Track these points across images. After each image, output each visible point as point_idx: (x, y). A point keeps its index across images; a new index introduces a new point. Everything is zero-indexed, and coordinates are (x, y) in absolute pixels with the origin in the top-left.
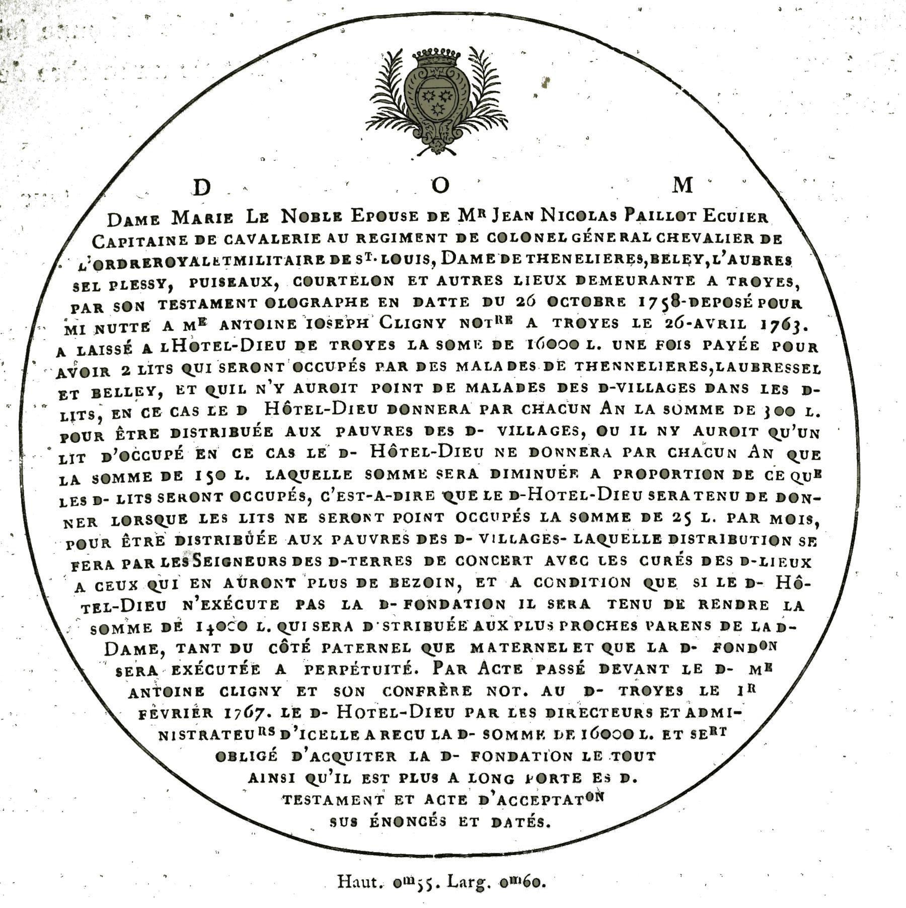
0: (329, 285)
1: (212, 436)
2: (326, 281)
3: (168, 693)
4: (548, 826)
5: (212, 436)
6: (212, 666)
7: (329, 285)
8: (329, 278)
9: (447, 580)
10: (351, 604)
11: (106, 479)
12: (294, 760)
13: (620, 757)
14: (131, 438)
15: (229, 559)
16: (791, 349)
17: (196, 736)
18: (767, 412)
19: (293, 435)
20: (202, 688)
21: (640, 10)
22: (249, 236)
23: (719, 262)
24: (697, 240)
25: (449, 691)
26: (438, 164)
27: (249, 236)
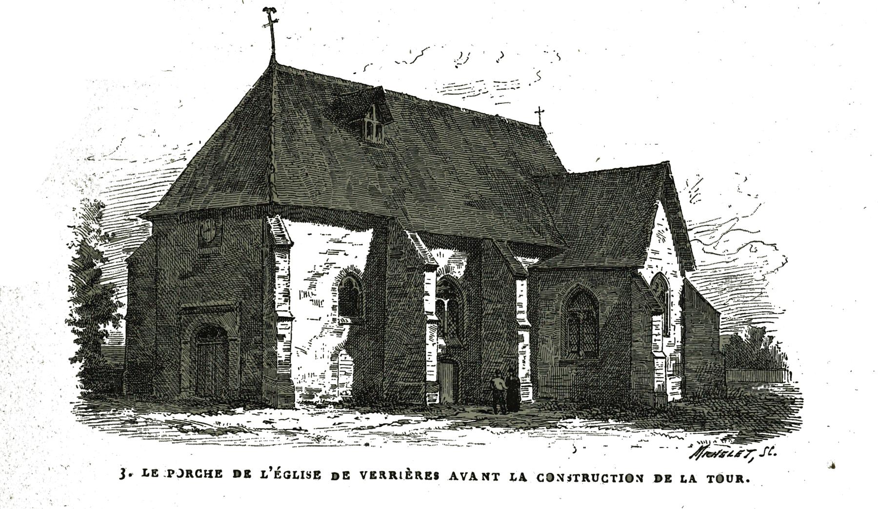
0: (737, 481)
1: (584, 481)
2: (735, 479)
3: (720, 480)
4: (748, 481)
5: (584, 481)
6: (201, 471)
7: (737, 481)
8: (737, 476)
9: (484, 474)
10: (517, 476)
11: (629, 479)
12: (235, 476)
13: (714, 480)
14: (614, 481)
15: (289, 472)
16: (723, 480)
17: (580, 478)
18: (123, 473)
19: (456, 479)
20: (221, 471)
21: (833, 467)
22: (462, 474)
23: (267, 477)
24: (464, 479)
25: (413, 475)
26: (327, 291)
27: (462, 474)
